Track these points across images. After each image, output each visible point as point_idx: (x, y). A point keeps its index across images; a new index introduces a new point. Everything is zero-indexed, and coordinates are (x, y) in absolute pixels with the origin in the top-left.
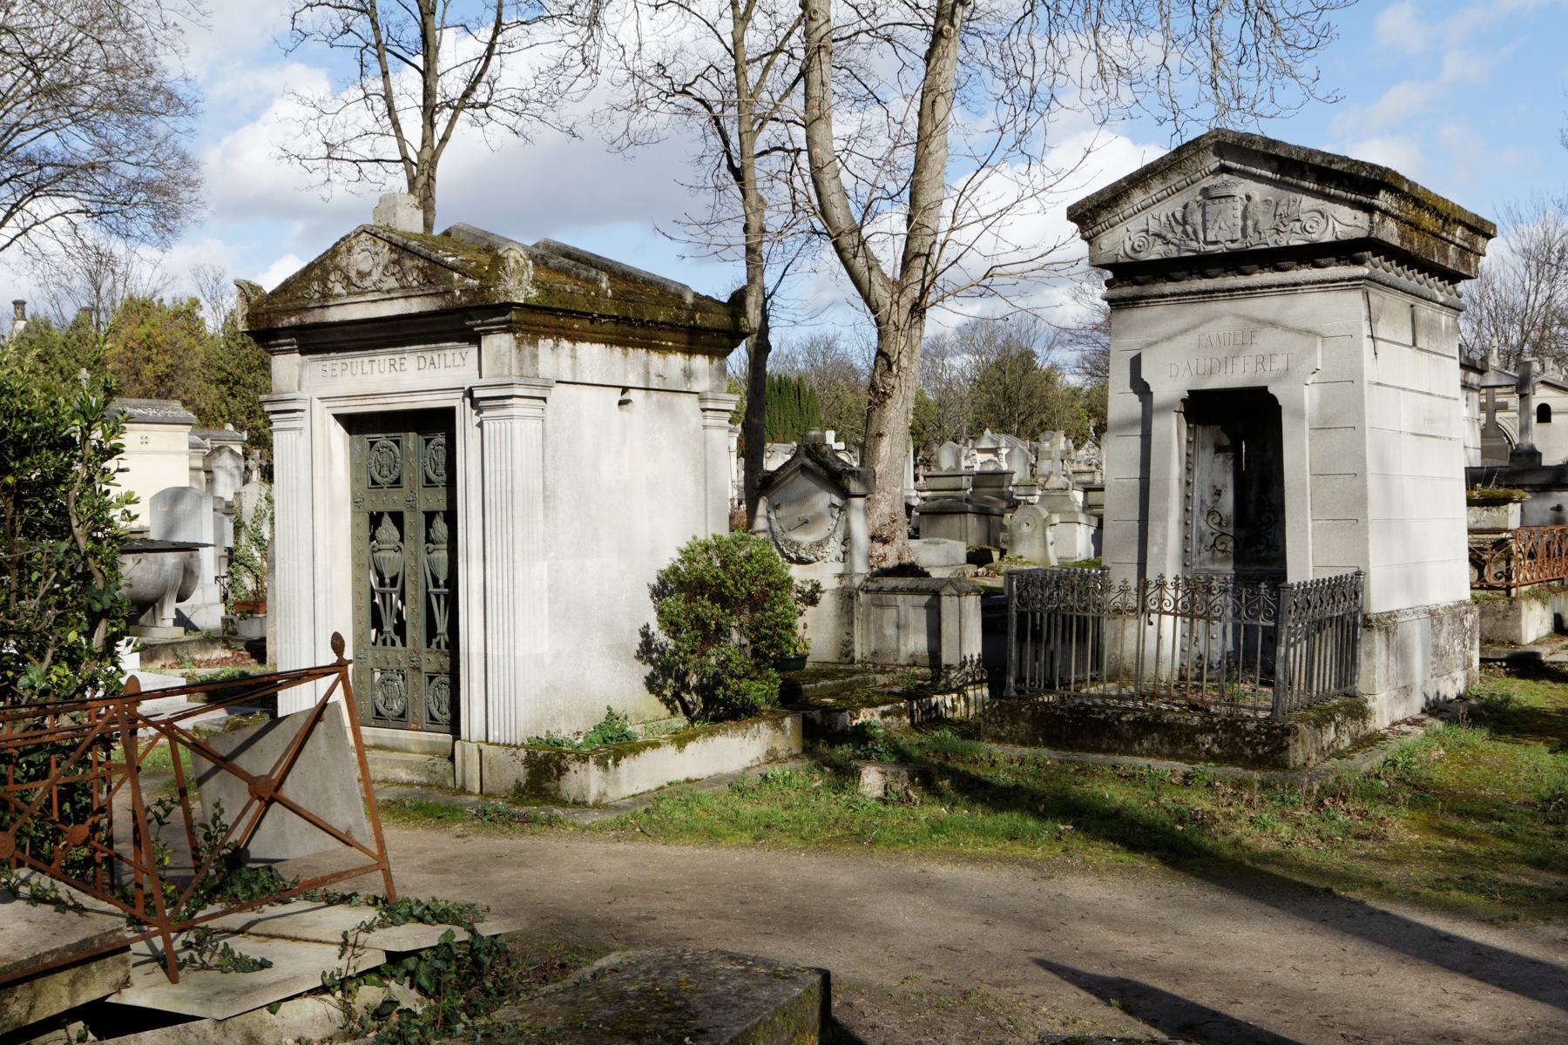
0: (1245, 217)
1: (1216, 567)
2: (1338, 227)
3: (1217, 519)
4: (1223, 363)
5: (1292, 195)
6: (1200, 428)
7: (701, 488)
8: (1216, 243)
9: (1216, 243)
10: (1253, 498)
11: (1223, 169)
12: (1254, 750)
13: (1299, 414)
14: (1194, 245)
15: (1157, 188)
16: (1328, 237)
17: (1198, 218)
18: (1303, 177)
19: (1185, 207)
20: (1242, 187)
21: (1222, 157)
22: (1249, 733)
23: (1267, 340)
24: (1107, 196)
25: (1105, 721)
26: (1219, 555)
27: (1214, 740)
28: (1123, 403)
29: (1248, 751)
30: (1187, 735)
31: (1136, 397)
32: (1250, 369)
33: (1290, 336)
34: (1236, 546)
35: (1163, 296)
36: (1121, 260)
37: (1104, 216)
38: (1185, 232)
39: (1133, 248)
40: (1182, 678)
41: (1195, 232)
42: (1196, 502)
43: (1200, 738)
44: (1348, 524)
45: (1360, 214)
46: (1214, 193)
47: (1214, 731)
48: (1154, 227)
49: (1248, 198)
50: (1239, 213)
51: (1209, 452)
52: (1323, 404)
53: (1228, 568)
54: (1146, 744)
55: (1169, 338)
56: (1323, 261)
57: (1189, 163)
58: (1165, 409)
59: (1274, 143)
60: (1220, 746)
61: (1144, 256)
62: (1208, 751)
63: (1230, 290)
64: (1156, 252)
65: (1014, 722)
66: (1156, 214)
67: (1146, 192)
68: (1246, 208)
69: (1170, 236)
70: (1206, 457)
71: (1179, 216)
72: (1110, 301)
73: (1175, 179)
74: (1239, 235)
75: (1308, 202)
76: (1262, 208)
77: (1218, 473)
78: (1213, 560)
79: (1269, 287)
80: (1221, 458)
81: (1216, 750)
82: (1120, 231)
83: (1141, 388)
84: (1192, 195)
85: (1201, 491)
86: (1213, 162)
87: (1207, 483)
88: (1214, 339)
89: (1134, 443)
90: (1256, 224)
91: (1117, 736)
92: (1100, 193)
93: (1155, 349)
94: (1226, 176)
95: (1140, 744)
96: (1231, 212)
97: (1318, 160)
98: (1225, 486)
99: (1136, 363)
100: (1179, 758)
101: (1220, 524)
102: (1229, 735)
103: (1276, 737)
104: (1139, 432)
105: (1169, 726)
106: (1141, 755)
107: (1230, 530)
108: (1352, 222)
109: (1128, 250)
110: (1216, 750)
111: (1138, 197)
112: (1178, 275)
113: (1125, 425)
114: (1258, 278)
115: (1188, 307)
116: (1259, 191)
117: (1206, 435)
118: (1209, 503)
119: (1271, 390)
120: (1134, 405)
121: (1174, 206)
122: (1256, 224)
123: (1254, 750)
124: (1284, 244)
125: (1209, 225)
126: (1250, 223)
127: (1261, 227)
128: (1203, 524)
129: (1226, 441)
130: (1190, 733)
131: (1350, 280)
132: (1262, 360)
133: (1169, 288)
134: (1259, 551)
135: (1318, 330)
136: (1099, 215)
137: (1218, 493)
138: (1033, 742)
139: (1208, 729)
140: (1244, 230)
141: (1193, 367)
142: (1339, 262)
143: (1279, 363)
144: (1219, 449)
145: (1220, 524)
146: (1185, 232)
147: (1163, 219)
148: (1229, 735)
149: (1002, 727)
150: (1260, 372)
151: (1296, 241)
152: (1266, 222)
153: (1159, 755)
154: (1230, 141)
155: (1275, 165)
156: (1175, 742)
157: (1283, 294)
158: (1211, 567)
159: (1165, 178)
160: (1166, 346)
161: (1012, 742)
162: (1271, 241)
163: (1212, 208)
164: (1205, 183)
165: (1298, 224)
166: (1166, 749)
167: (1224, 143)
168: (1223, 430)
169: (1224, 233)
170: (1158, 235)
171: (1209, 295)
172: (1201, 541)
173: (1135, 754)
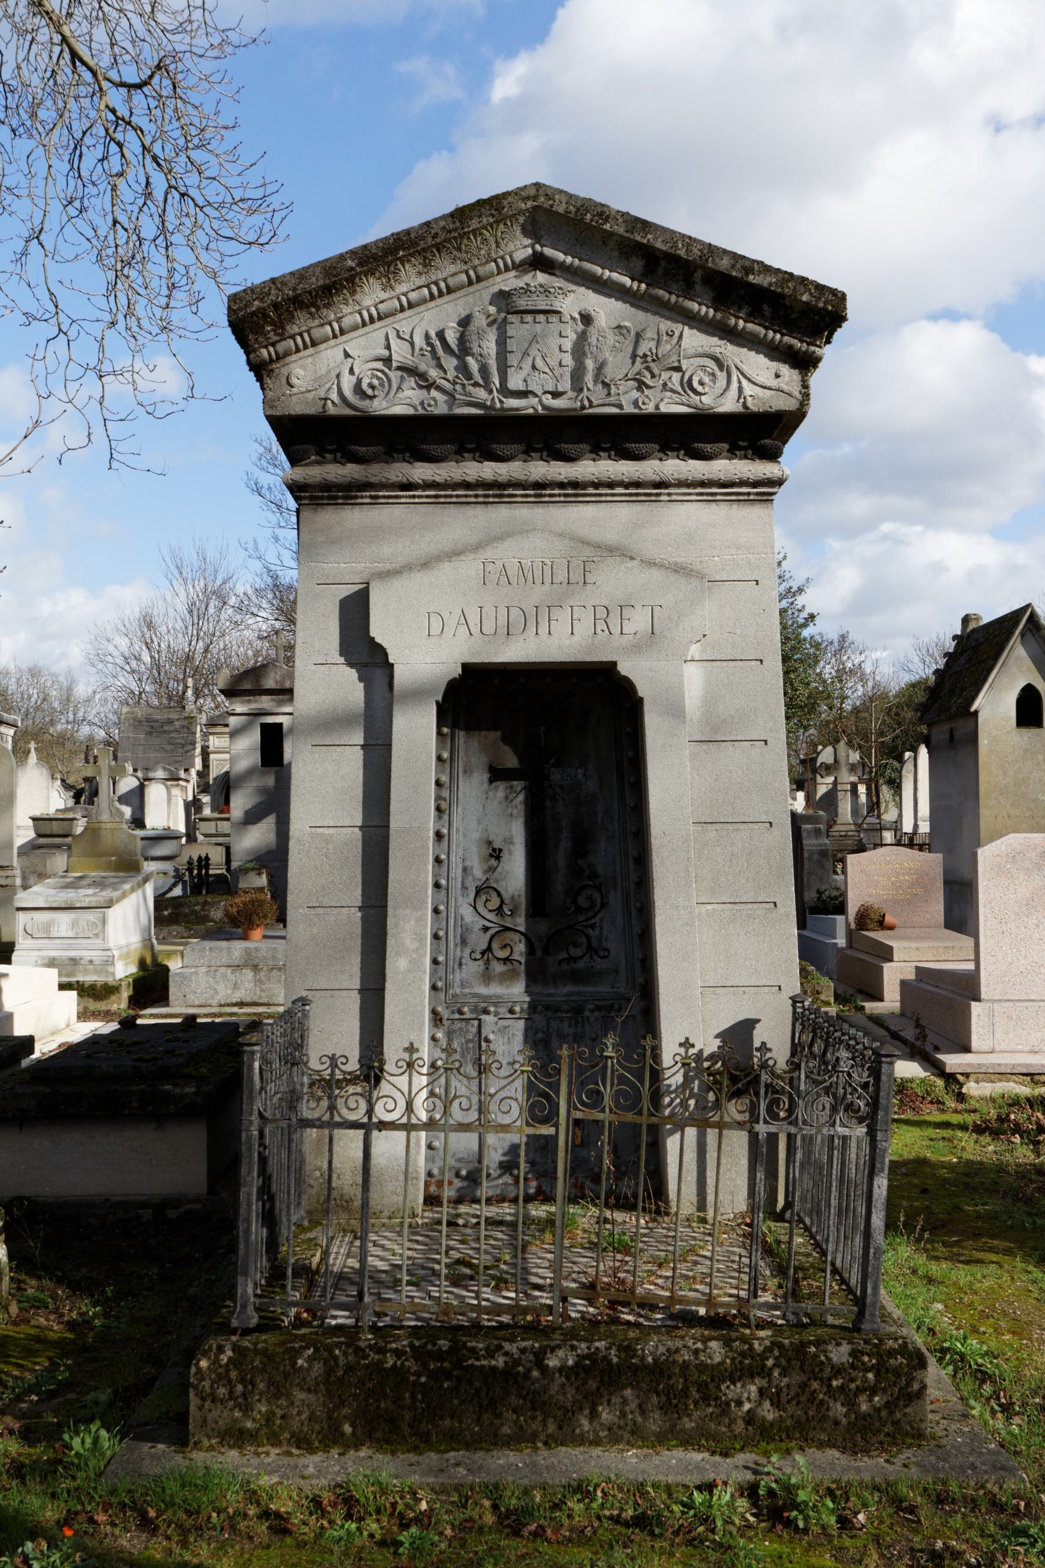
0: (579, 351)
1: (495, 989)
2: (748, 389)
3: (495, 903)
4: (534, 618)
5: (665, 325)
6: (461, 735)
7: (412, 1159)
8: (524, 394)
9: (524, 394)
10: (562, 863)
11: (539, 263)
12: (851, 1404)
13: (676, 711)
14: (481, 394)
15: (410, 280)
16: (729, 405)
17: (490, 346)
18: (688, 292)
19: (465, 322)
20: (576, 300)
21: (537, 238)
22: (838, 1371)
23: (613, 580)
24: (316, 282)
25: (508, 1374)
26: (498, 968)
27: (761, 1392)
28: (325, 681)
29: (838, 1409)
30: (702, 1386)
31: (352, 674)
32: (584, 628)
33: (656, 574)
34: (531, 950)
35: (408, 486)
36: (332, 410)
37: (301, 322)
38: (464, 369)
39: (358, 389)
40: (432, 1200)
41: (484, 370)
42: (457, 872)
43: (731, 1391)
44: (760, 910)
45: (785, 370)
46: (523, 303)
47: (764, 1372)
48: (400, 353)
49: (587, 319)
50: (568, 345)
51: (480, 777)
52: (709, 700)
53: (517, 991)
54: (606, 1415)
55: (425, 564)
56: (708, 448)
57: (476, 242)
58: (416, 694)
59: (645, 225)
60: (776, 1404)
61: (380, 406)
62: (750, 1419)
63: (539, 486)
64: (403, 401)
65: (277, 1390)
66: (405, 328)
67: (388, 286)
68: (582, 337)
69: (434, 373)
70: (473, 790)
71: (451, 337)
72: (296, 488)
73: (447, 269)
74: (565, 385)
75: (693, 340)
76: (611, 338)
77: (492, 819)
78: (487, 977)
79: (611, 485)
80: (501, 790)
81: (768, 1413)
82: (330, 355)
83: (365, 654)
84: (478, 302)
85: (467, 851)
86: (521, 248)
87: (476, 835)
88: (513, 571)
89: (919, 815)
90: (600, 368)
91: (537, 1403)
92: (301, 275)
93: (397, 584)
94: (541, 277)
95: (594, 1415)
96: (554, 342)
97: (724, 264)
98: (509, 841)
99: (355, 610)
100: (687, 1442)
101: (499, 911)
102: (797, 1378)
103: (897, 1372)
104: (358, 737)
105: (660, 1370)
106: (596, 1442)
107: (520, 923)
108: (773, 383)
109: (348, 393)
110: (768, 1413)
111: (372, 294)
112: (436, 450)
113: (328, 724)
114: (587, 468)
115: (452, 510)
116: (607, 311)
117: (471, 748)
118: (478, 873)
119: (623, 669)
120: (346, 687)
121: (441, 317)
122: (600, 368)
123: (851, 1404)
124: (650, 408)
125: (513, 360)
126: (590, 364)
127: (609, 373)
128: (467, 913)
129: (511, 761)
130: (708, 1383)
131: (756, 484)
132: (604, 615)
133: (421, 472)
134: (575, 959)
135: (697, 567)
136: (291, 319)
137: (496, 854)
138: (329, 1437)
139: (747, 1367)
140: (577, 376)
141: (474, 620)
142: (733, 452)
143: (638, 622)
144: (497, 774)
145: (499, 911)
146: (464, 369)
147: (419, 341)
148: (797, 1378)
149: (247, 1409)
150: (603, 636)
151: (671, 406)
152: (618, 366)
153: (637, 1436)
154: (561, 209)
155: (638, 264)
156: (673, 1404)
157: (633, 500)
158: (483, 990)
159: (427, 264)
160: (419, 580)
161: (274, 1440)
162: (628, 400)
163: (518, 330)
164: (510, 281)
165: (676, 376)
166: (655, 1423)
167: (550, 212)
168: (506, 740)
169: (540, 378)
170: (408, 370)
171: (497, 491)
172: (464, 942)
173: (581, 1440)
